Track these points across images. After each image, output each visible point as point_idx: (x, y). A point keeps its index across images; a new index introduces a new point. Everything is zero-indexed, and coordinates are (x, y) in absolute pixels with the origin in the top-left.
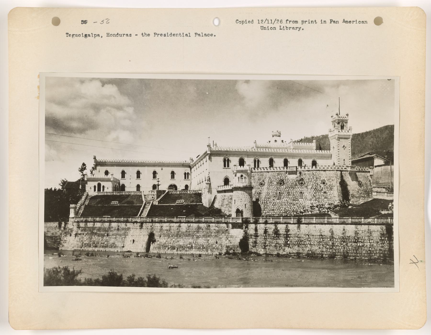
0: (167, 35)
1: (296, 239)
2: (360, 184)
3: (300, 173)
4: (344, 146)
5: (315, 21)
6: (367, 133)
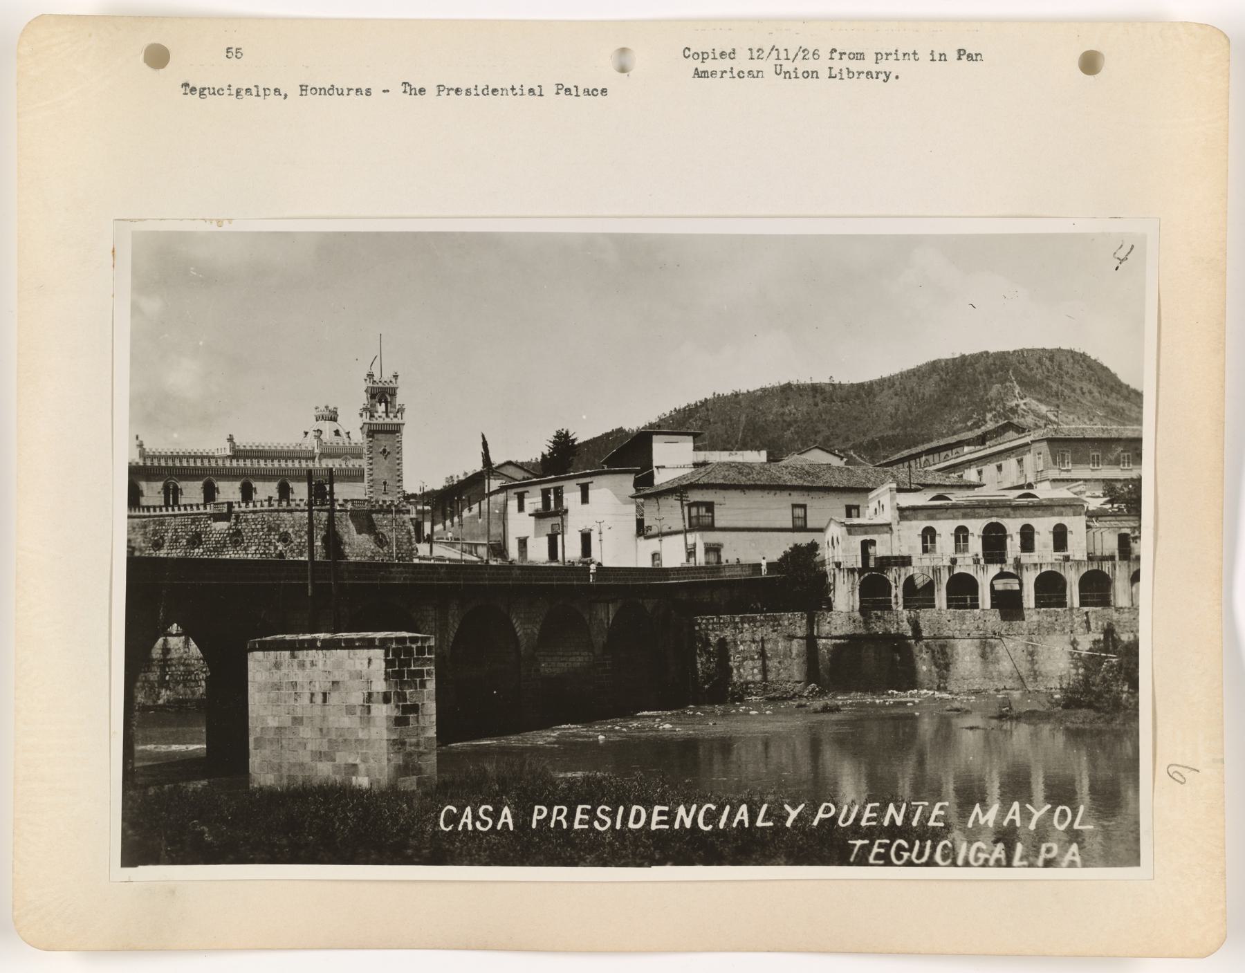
0: (474, 92)
1: (182, 668)
2: (381, 541)
3: (237, 517)
4: (384, 451)
5: (915, 53)
6: (882, 382)
